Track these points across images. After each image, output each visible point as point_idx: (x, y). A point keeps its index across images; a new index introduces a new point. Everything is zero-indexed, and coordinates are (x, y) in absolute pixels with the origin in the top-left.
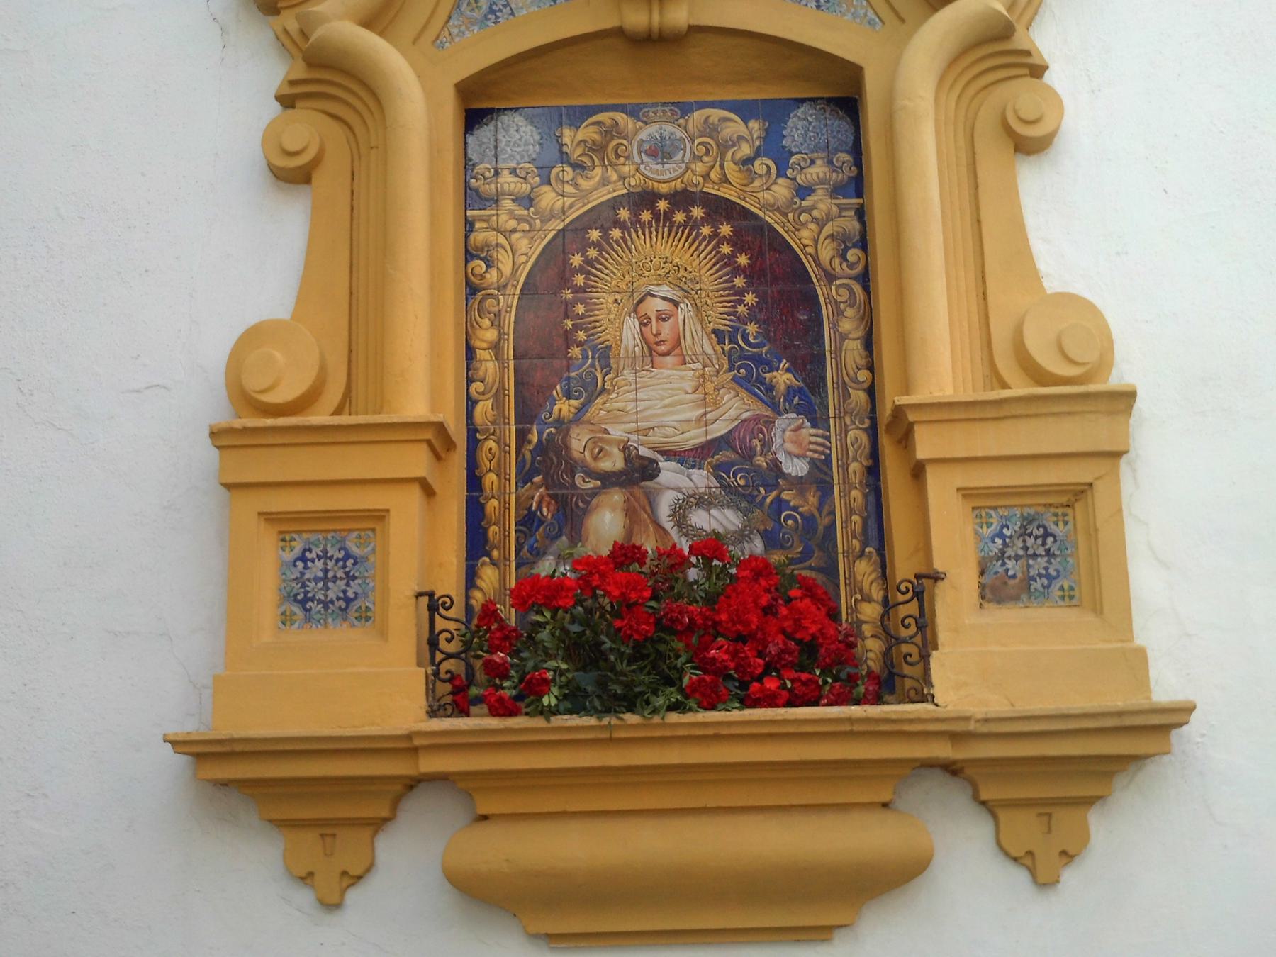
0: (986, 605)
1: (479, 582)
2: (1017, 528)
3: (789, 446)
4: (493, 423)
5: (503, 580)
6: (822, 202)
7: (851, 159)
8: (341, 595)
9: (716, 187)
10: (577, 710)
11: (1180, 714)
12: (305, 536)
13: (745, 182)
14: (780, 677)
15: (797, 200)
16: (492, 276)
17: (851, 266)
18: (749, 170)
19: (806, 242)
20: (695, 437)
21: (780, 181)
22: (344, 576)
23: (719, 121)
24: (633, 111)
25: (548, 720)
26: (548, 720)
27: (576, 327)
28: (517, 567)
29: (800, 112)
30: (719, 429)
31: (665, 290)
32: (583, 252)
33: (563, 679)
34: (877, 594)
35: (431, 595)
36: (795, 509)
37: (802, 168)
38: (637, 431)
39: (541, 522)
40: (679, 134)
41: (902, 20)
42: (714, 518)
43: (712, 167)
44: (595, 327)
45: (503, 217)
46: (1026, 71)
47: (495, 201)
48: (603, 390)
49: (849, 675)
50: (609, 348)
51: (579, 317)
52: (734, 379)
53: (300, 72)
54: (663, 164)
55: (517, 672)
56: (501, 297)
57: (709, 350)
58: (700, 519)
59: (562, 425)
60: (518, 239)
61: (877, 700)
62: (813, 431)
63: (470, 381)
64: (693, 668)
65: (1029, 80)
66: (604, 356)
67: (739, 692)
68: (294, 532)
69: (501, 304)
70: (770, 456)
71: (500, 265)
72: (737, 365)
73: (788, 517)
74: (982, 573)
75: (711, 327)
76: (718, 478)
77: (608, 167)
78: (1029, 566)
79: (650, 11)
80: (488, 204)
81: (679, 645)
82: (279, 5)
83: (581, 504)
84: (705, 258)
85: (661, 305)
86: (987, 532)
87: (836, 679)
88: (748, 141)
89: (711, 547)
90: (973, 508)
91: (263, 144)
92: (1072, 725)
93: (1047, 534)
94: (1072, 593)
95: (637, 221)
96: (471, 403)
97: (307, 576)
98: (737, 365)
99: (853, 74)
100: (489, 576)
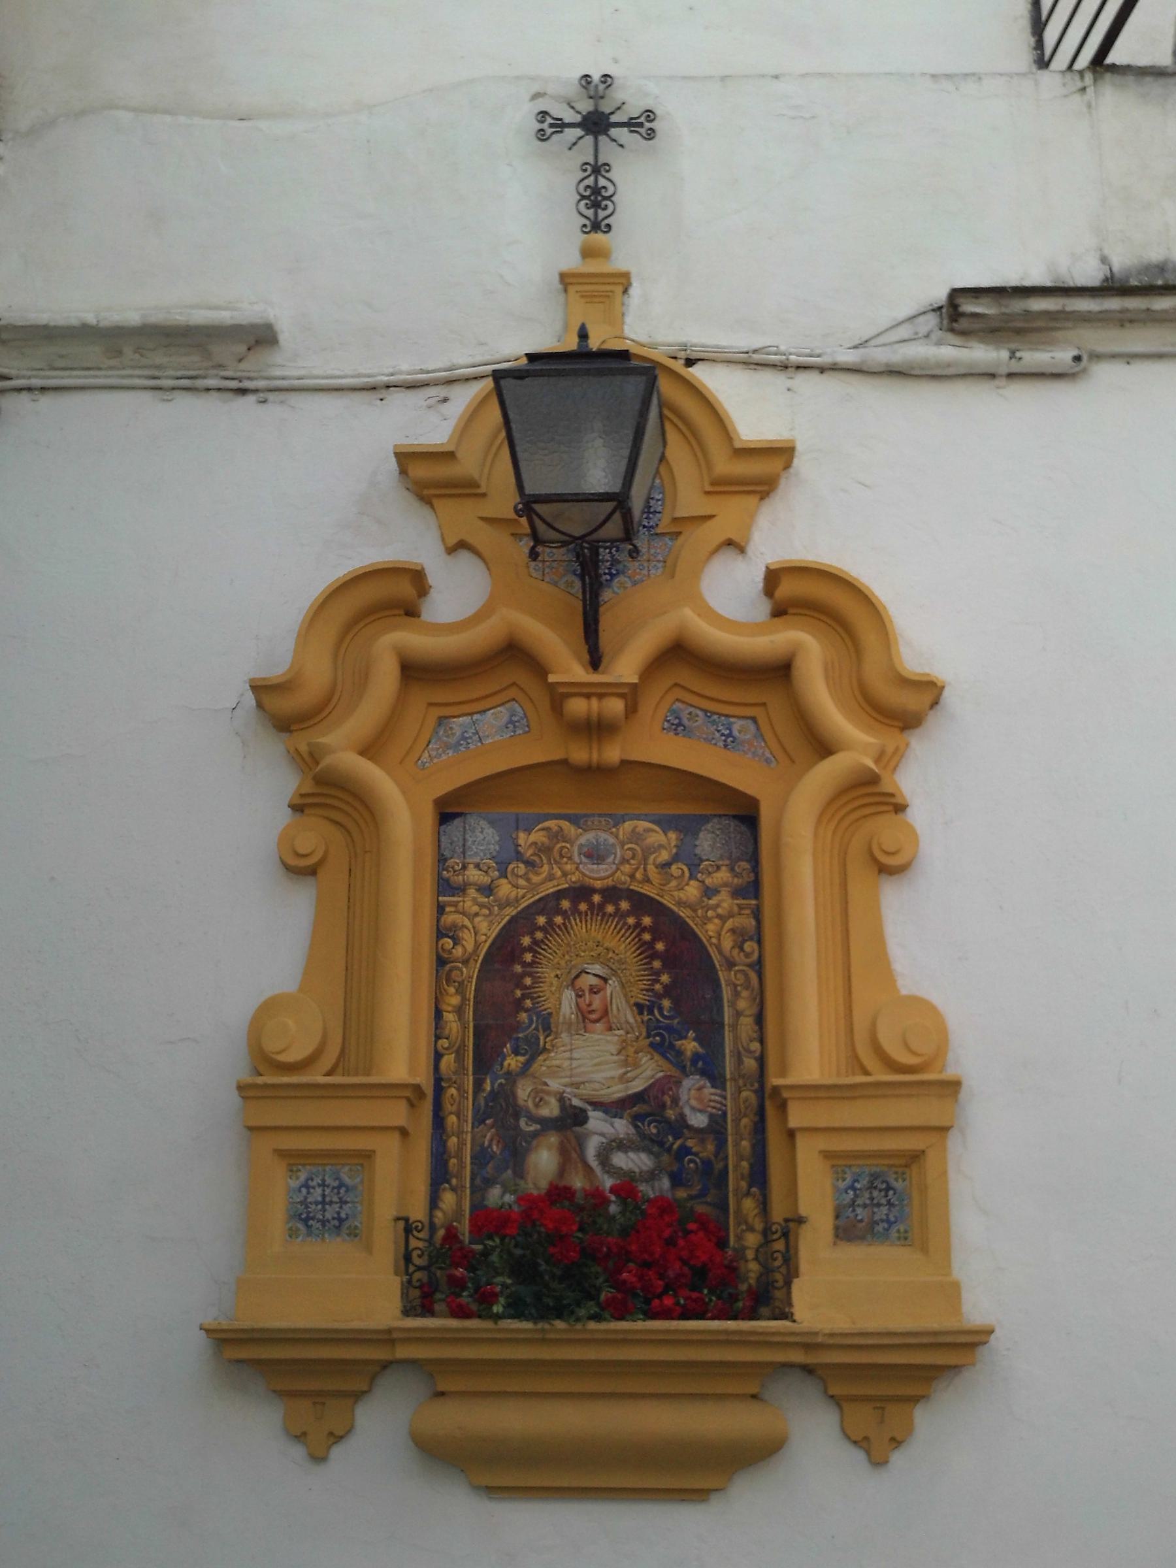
0: (839, 1242)
1: (441, 1205)
2: (865, 1182)
3: (693, 1103)
4: (455, 1073)
5: (459, 1203)
6: (725, 901)
7: (749, 867)
8: (336, 1216)
9: (640, 886)
10: (519, 1315)
11: (985, 1333)
12: (308, 1167)
13: (664, 882)
14: (676, 1295)
15: (705, 899)
16: (458, 952)
17: (747, 955)
18: (666, 873)
19: (711, 933)
20: (617, 1092)
21: (692, 882)
22: (338, 1200)
23: (644, 831)
24: (574, 820)
25: (496, 1323)
26: (496, 1323)
27: (524, 997)
28: (472, 1193)
29: (709, 826)
30: (638, 1086)
31: (597, 969)
32: (532, 934)
33: (508, 1291)
34: (759, 1225)
35: (407, 1220)
36: (696, 1154)
37: (710, 873)
38: (571, 1085)
39: (492, 1157)
40: (612, 840)
41: (793, 762)
42: (632, 1160)
43: (637, 869)
44: (539, 997)
45: (468, 904)
46: (891, 808)
47: (461, 890)
48: (545, 1050)
49: (730, 1295)
50: (550, 1014)
51: (527, 988)
52: (651, 1045)
53: (308, 788)
54: (598, 864)
55: (473, 1284)
56: (464, 969)
57: (631, 1020)
58: (620, 1160)
59: (511, 1078)
60: (479, 922)
61: (752, 1315)
62: (713, 1090)
63: (438, 1037)
64: (610, 1287)
65: (892, 816)
66: (547, 1024)
67: (643, 1305)
68: (300, 1164)
69: (464, 975)
70: (678, 1110)
71: (464, 942)
72: (652, 1033)
73: (691, 1161)
74: (837, 1217)
75: (632, 1001)
76: (636, 1127)
77: (554, 866)
78: (874, 1213)
79: (591, 748)
80: (456, 892)
81: (599, 1269)
82: (292, 728)
83: (524, 1144)
84: (629, 943)
85: (594, 981)
86: (842, 1185)
87: (719, 1298)
88: (666, 849)
89: (626, 1189)
90: (833, 1166)
91: (278, 844)
92: (897, 1341)
93: (889, 1188)
94: (906, 1235)
95: (575, 910)
96: (438, 1056)
97: (309, 1200)
98: (652, 1033)
99: (754, 803)
100: (448, 1199)
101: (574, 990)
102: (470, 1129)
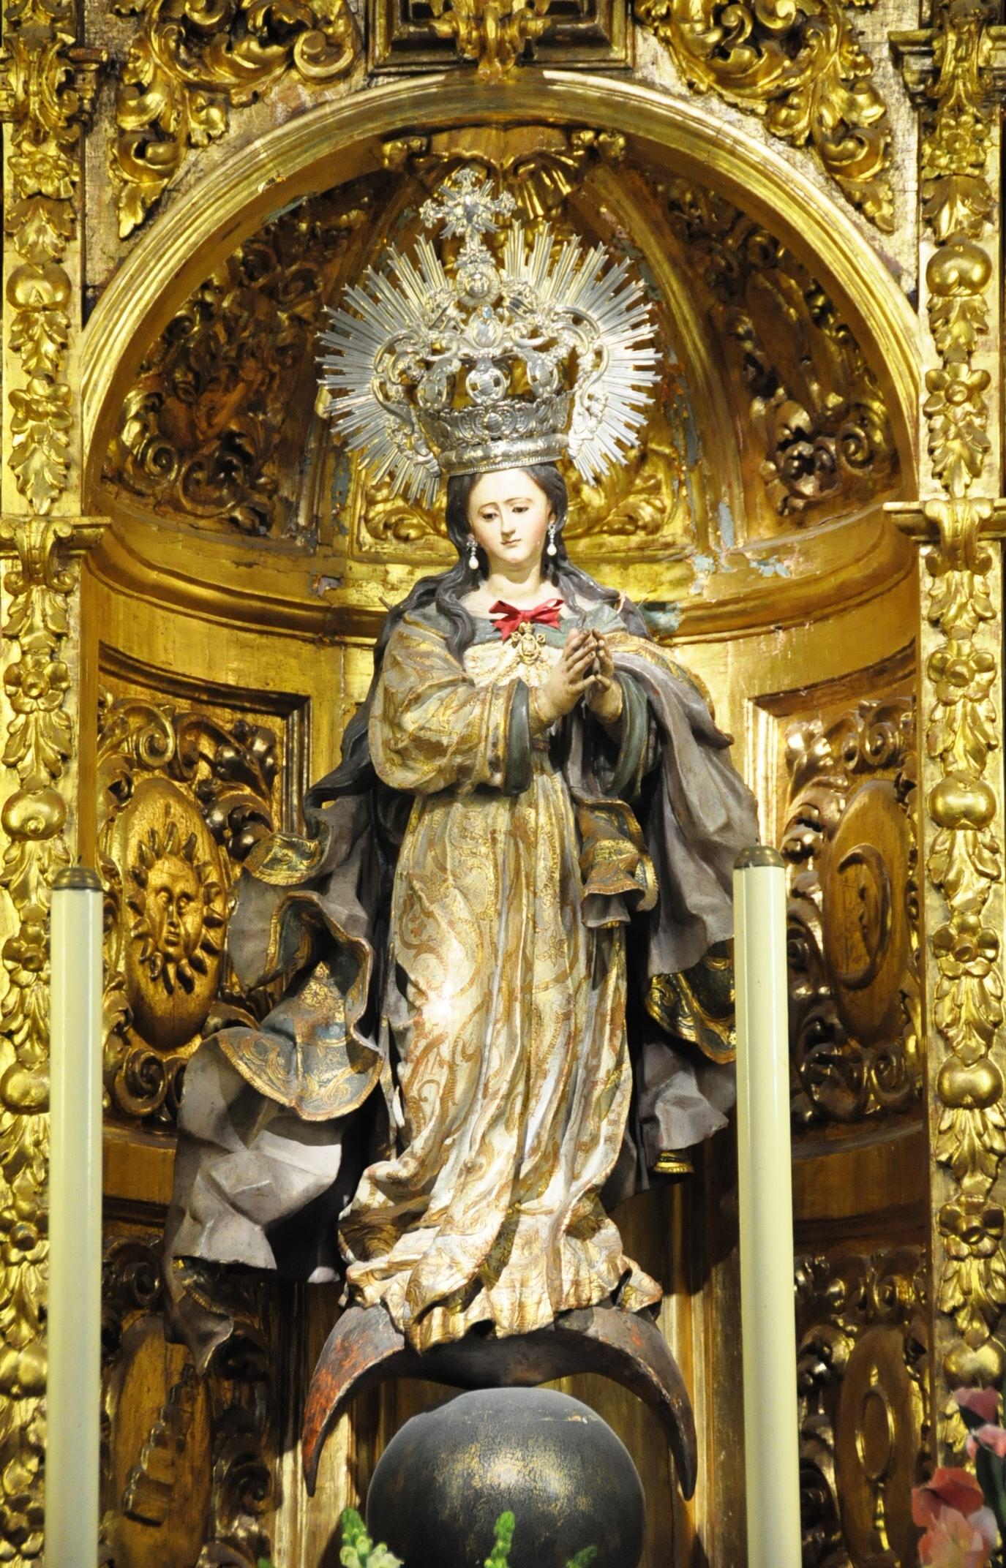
101: (513, 816)
102: (540, 211)
